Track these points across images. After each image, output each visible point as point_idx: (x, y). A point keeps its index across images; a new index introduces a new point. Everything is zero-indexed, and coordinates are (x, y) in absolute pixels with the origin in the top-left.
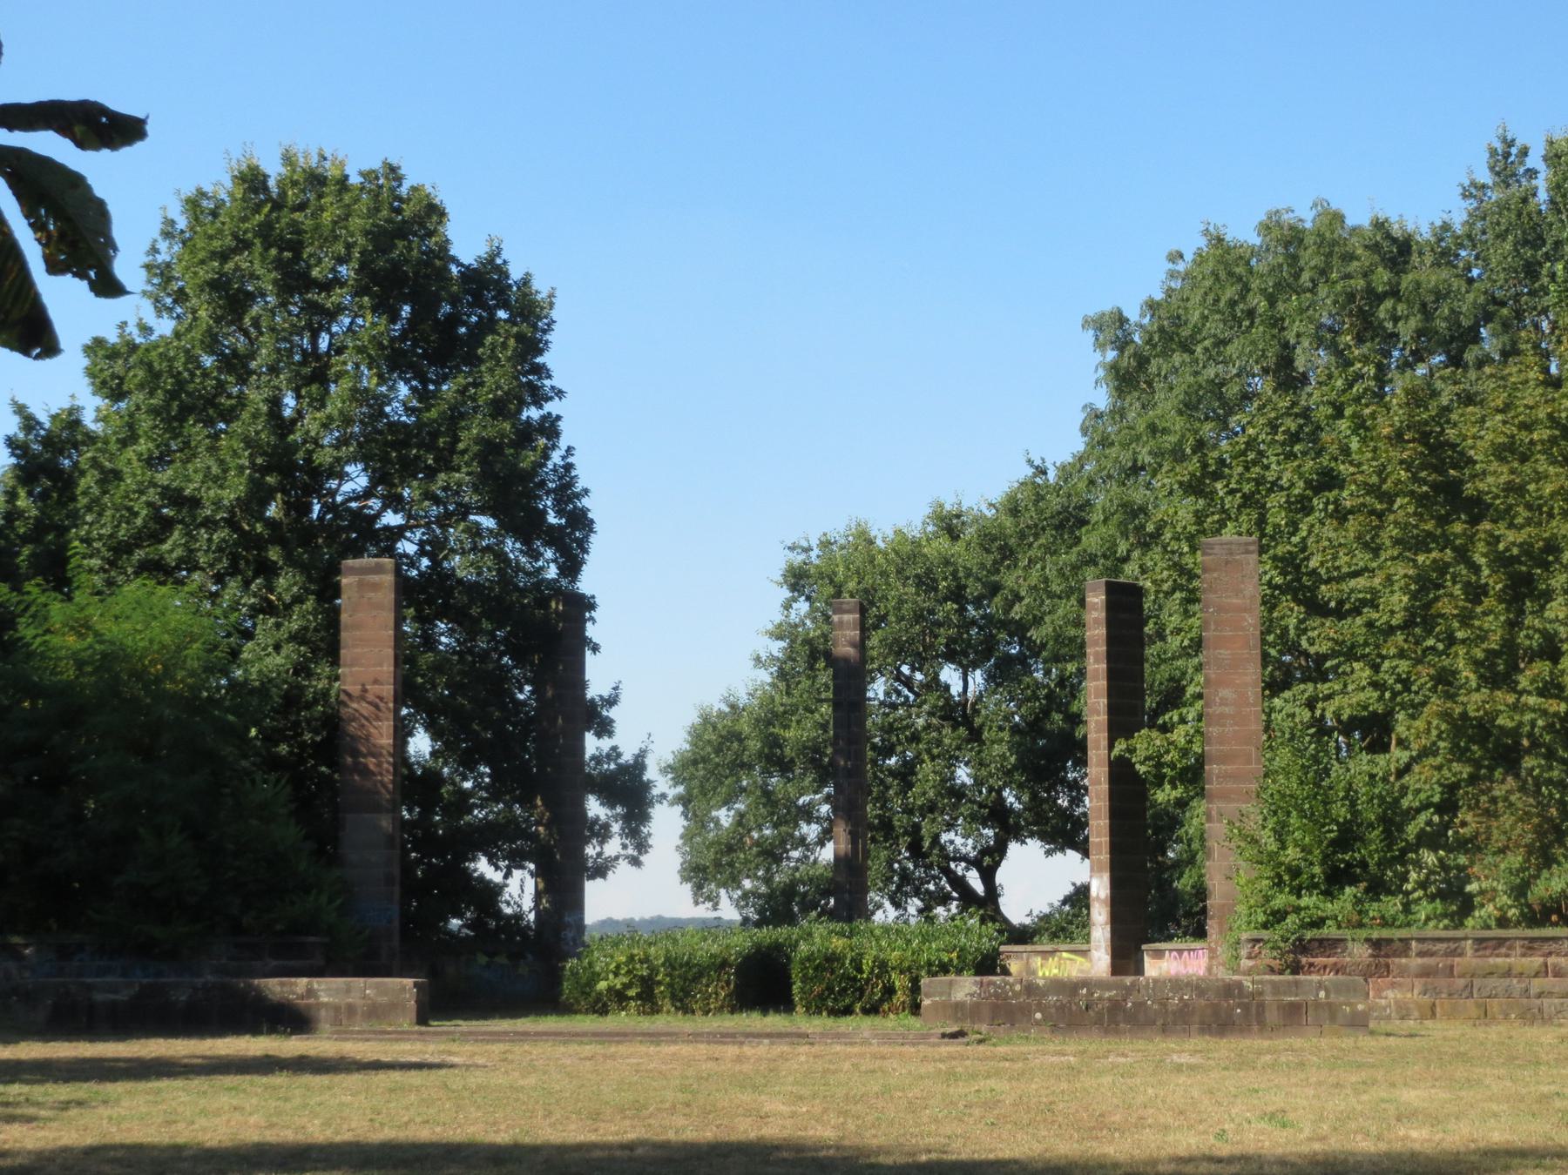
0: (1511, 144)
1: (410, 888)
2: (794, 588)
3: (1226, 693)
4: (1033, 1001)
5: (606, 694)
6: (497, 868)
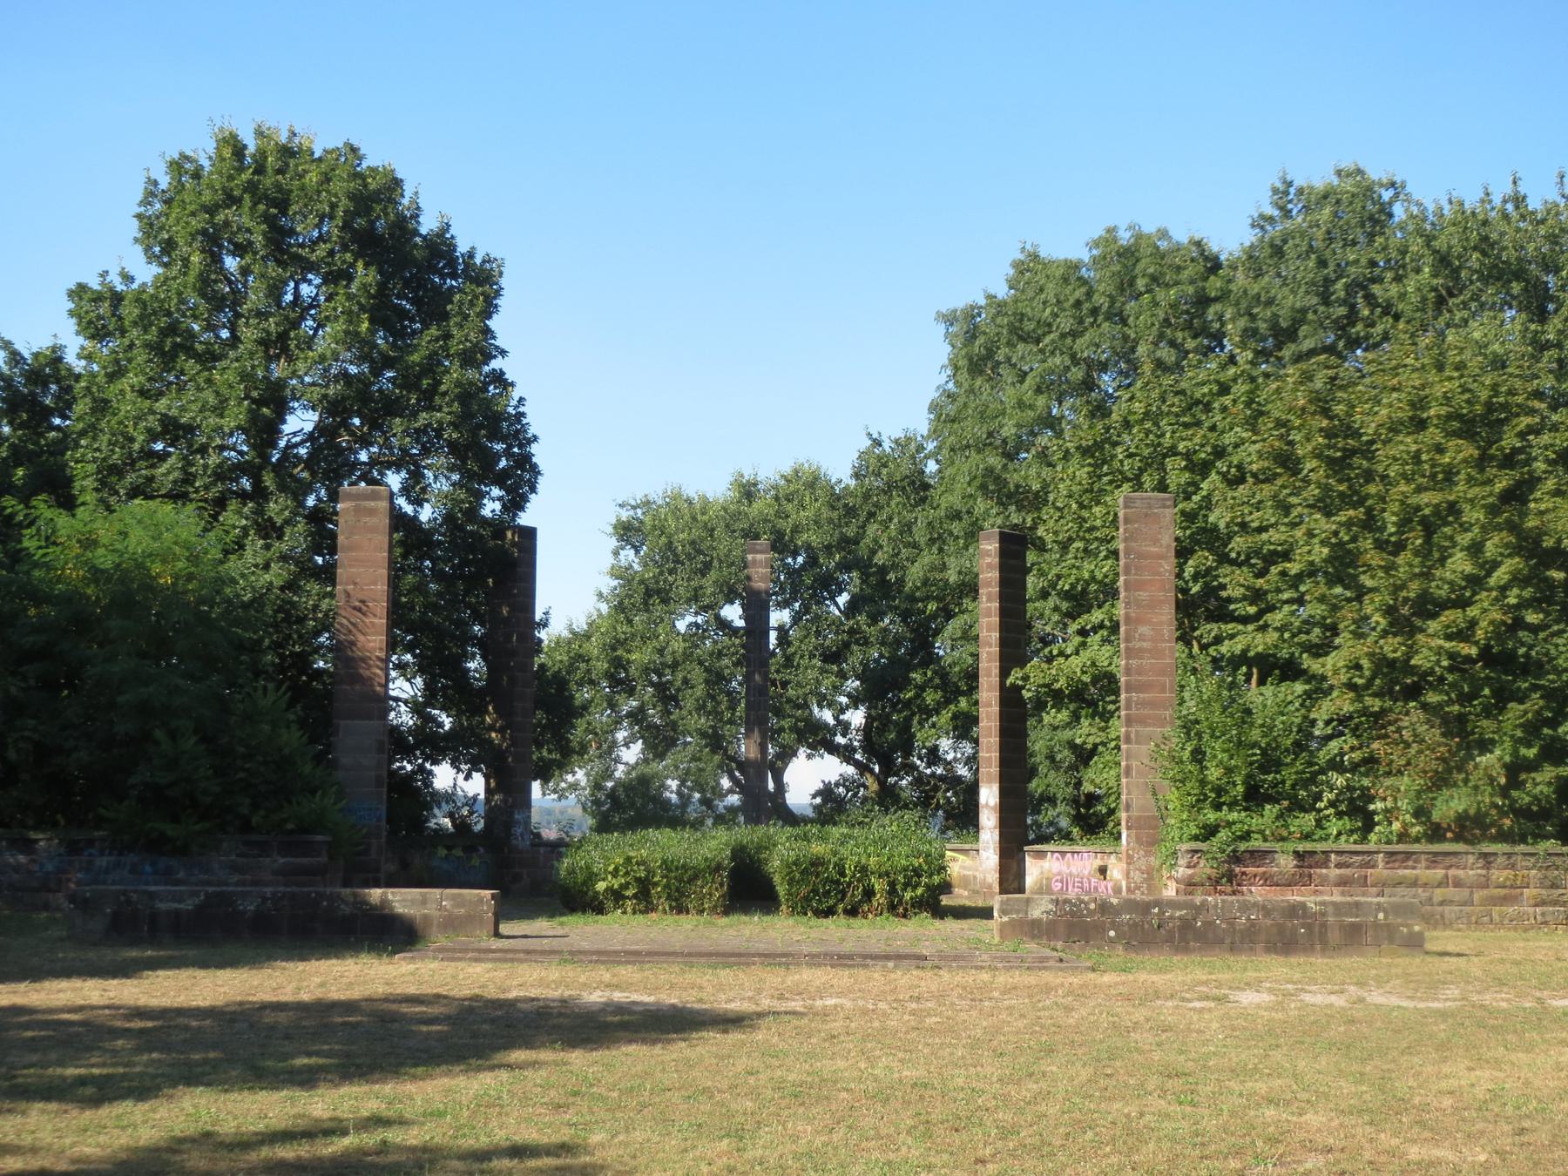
0: (1290, 184)
2: (621, 539)
3: (1144, 630)
4: (1107, 919)
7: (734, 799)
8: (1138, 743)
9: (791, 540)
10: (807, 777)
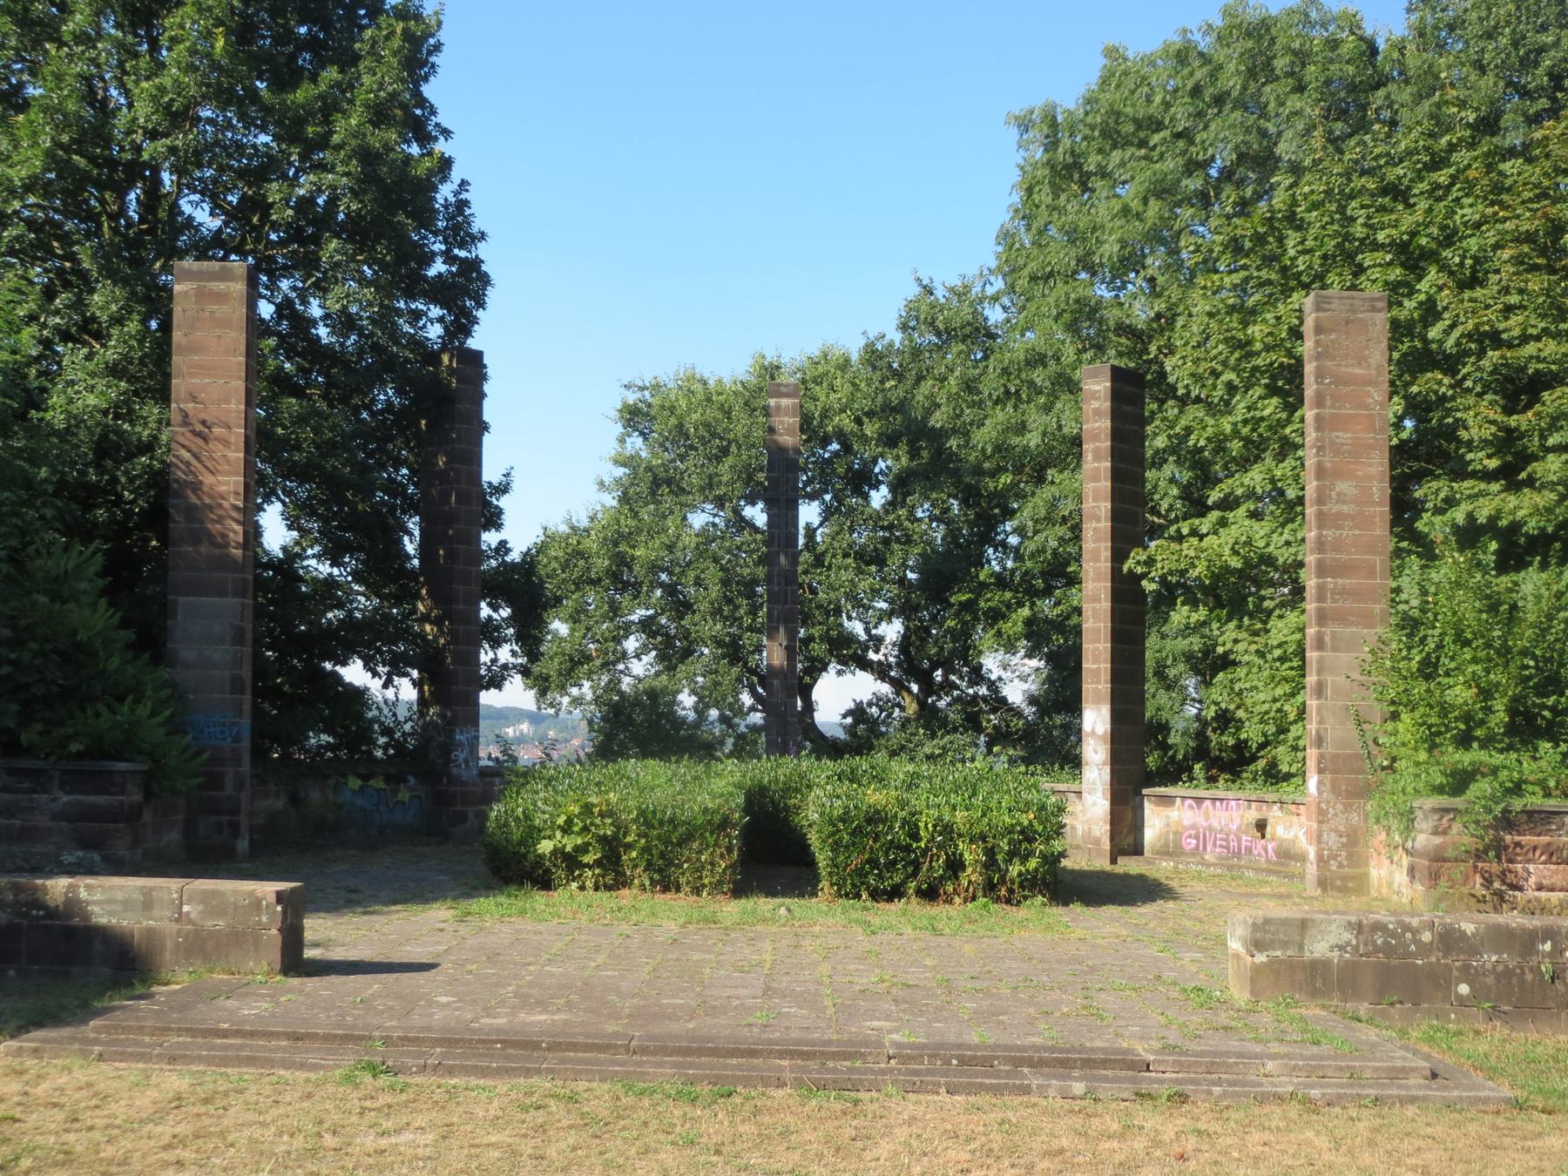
1: (264, 691)
3: (1343, 486)
5: (495, 482)
6: (375, 674)
7: (757, 718)
8: (1334, 649)
9: (821, 425)
10: (837, 695)
